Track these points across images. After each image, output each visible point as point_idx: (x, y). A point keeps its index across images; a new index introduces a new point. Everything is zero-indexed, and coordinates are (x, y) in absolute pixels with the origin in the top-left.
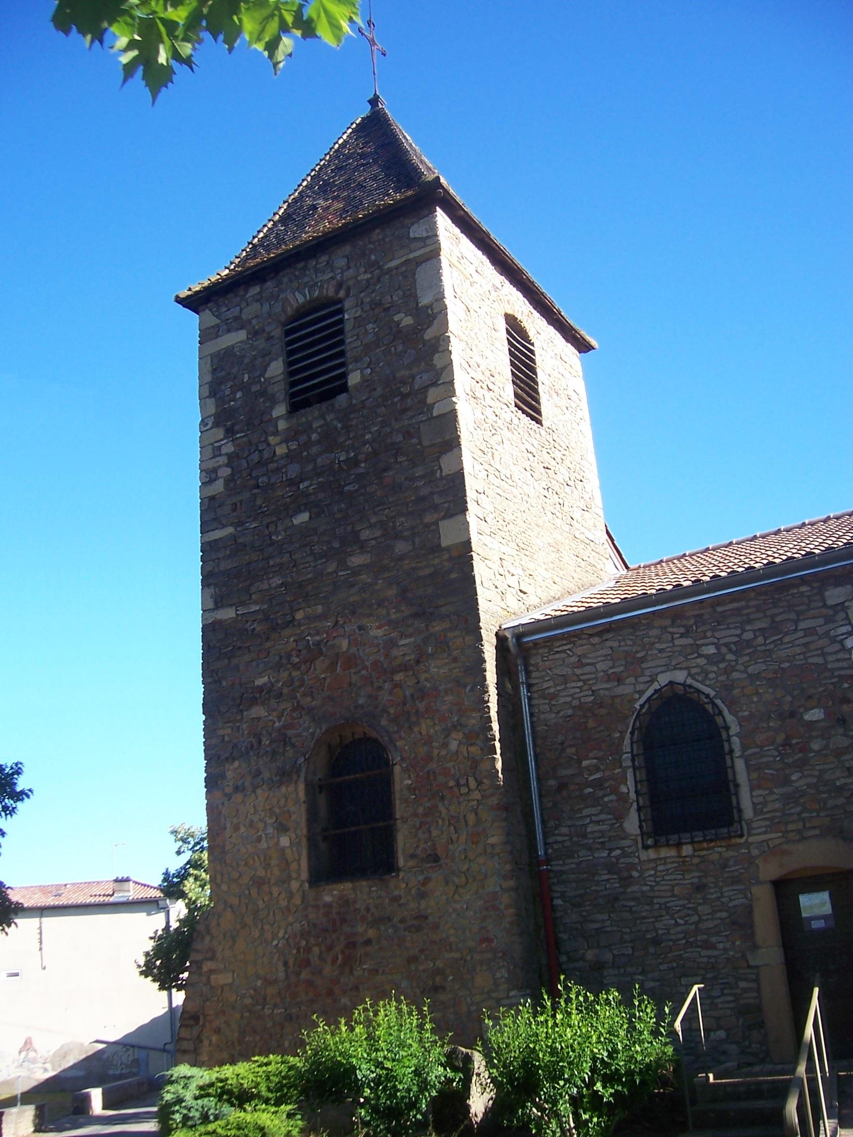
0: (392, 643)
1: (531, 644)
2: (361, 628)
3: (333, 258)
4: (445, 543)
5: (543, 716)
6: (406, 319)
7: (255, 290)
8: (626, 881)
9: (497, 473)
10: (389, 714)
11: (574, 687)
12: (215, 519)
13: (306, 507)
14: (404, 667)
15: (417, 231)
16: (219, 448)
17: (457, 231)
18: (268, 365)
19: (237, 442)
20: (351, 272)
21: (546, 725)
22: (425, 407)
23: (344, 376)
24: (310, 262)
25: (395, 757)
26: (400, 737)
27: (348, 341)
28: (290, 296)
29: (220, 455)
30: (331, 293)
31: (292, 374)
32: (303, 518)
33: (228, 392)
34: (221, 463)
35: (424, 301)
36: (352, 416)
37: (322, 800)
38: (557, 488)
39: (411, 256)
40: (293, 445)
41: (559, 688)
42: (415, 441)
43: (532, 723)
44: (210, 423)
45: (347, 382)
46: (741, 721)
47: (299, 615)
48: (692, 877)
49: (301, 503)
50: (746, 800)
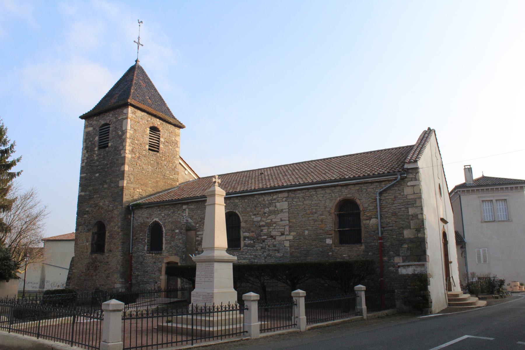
0: (109, 206)
7: (95, 118)
8: (144, 259)
14: (110, 211)
15: (125, 111)
22: (120, 154)
23: (108, 143)
25: (107, 229)
30: (108, 122)
32: (97, 175)
35: (124, 129)
37: (96, 236)
46: (166, 230)
47: (95, 196)
48: (154, 260)
50: (164, 246)
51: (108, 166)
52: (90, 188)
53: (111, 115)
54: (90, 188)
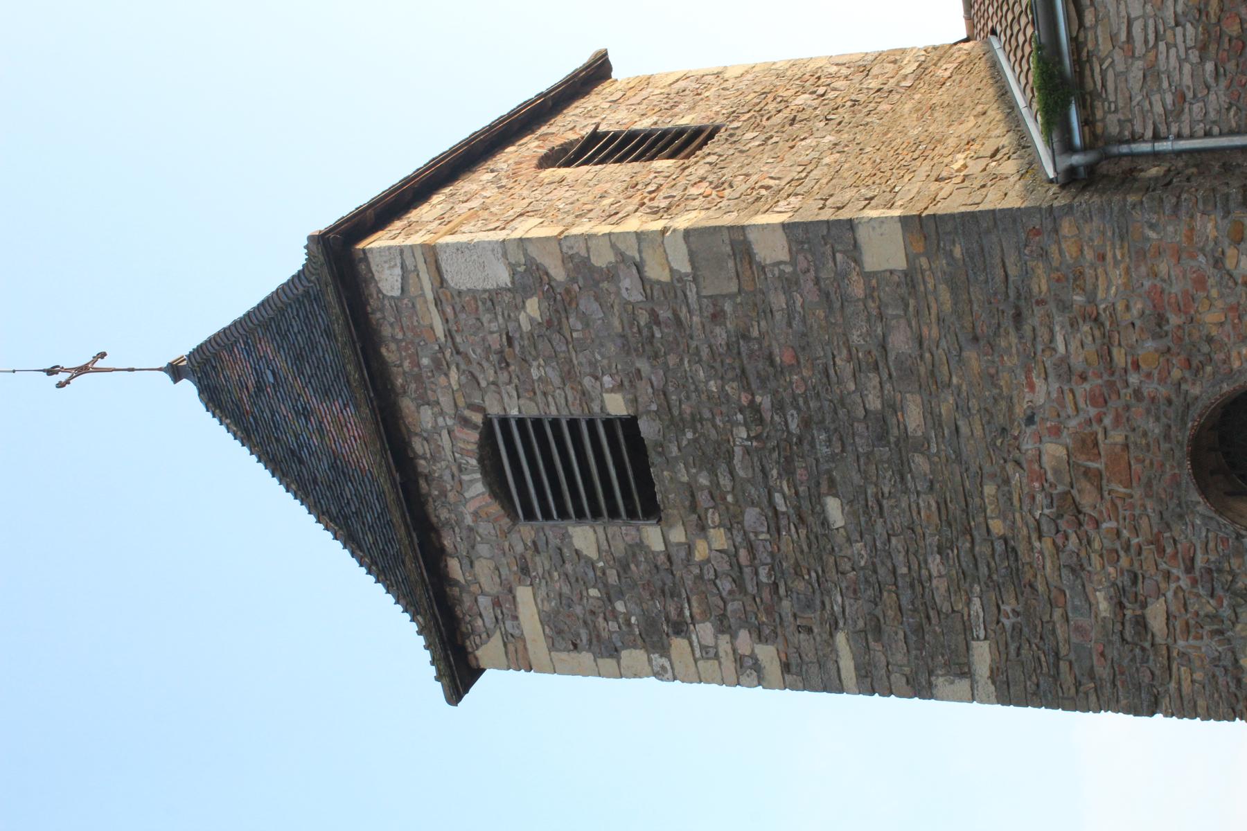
0: (1066, 371)
1: (1086, 129)
2: (1030, 420)
3: (418, 430)
4: (900, 263)
5: (1212, 115)
6: (528, 310)
7: (455, 568)
9: (794, 183)
10: (1183, 379)
11: (1167, 57)
12: (821, 666)
13: (816, 499)
16: (703, 648)
17: (398, 224)
18: (577, 552)
19: (698, 617)
20: (445, 401)
21: (1228, 109)
22: (674, 288)
23: (609, 423)
24: (420, 469)
26: (1224, 362)
27: (553, 412)
28: (471, 507)
29: (716, 647)
30: (474, 436)
31: (596, 514)
32: (834, 509)
33: (613, 626)
34: (728, 648)
36: (676, 412)
38: (826, 110)
39: (430, 296)
40: (713, 517)
41: (1165, 85)
42: (728, 307)
43: (1221, 134)
44: (658, 660)
45: (621, 419)
47: (997, 526)
49: (807, 511)
51: (764, 400)
52: (940, 585)
53: (426, 417)
54: (940, 585)
